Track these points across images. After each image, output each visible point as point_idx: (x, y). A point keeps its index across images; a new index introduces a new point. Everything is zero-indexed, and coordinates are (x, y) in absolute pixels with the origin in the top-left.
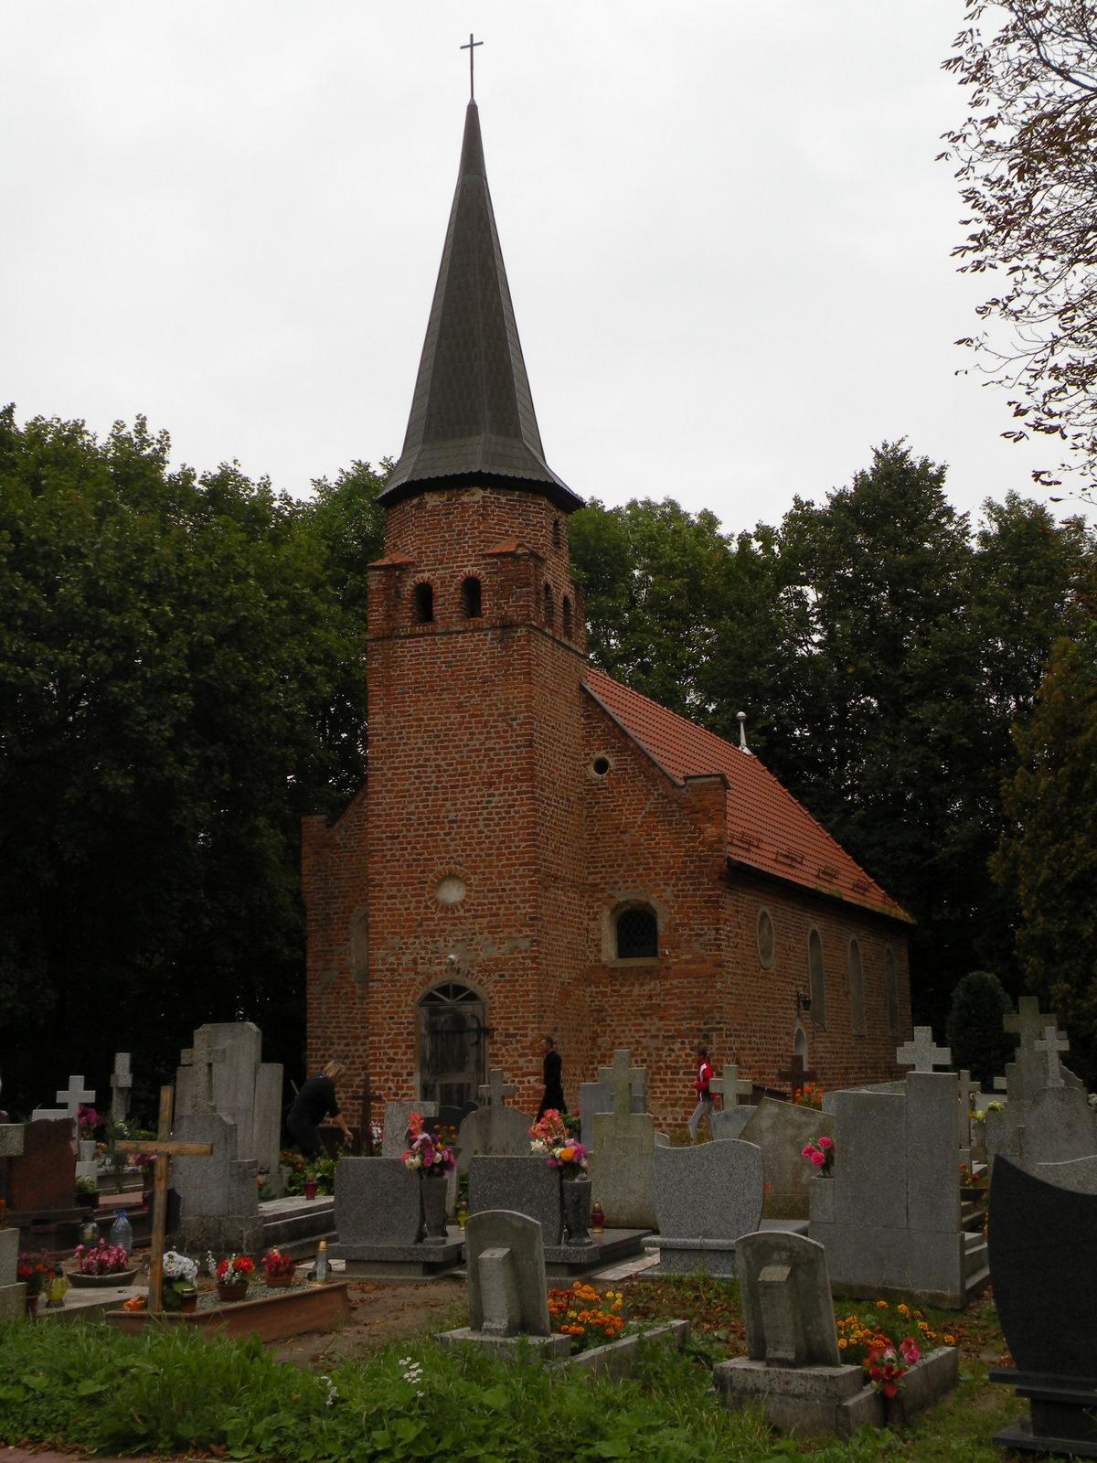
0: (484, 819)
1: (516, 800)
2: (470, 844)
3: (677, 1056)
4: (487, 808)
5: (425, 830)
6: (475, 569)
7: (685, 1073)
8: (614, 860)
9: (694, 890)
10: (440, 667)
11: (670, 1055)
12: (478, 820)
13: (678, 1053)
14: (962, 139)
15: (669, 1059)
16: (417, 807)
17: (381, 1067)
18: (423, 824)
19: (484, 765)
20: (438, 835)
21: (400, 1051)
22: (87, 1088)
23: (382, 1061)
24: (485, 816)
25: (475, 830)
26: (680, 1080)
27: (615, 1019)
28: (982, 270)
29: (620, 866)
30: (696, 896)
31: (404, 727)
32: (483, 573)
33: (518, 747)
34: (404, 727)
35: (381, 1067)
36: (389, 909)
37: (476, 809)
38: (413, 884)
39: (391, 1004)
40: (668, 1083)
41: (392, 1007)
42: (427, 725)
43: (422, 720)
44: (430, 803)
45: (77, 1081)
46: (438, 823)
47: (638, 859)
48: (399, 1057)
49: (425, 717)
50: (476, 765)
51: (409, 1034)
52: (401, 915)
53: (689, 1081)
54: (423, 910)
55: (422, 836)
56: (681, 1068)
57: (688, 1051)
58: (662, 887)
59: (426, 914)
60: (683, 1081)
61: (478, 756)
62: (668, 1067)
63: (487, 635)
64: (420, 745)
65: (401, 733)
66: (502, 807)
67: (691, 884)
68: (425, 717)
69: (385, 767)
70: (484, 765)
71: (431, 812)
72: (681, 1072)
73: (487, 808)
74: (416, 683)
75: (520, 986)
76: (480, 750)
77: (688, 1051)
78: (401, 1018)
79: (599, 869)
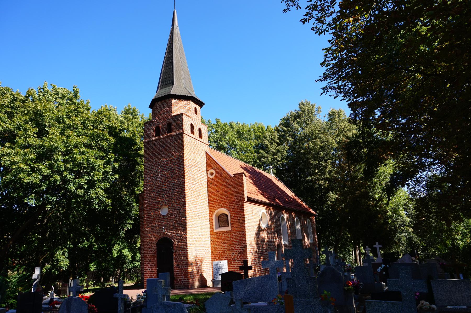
0: (173, 189)
1: (181, 183)
2: (169, 197)
3: (235, 256)
4: (173, 186)
5: (158, 194)
6: (170, 120)
7: (237, 261)
8: (216, 200)
9: (237, 206)
10: (161, 148)
11: (233, 255)
12: (171, 190)
13: (235, 255)
14: (317, 16)
15: (233, 256)
16: (156, 187)
17: (147, 263)
18: (157, 192)
19: (173, 174)
20: (161, 195)
21: (152, 258)
22: (379, 244)
23: (147, 261)
24: (173, 188)
25: (170, 193)
26: (236, 263)
27: (218, 245)
28: (286, 12)
29: (217, 201)
30: (238, 208)
31: (152, 165)
32: (172, 121)
33: (181, 168)
34: (152, 165)
35: (147, 263)
36: (149, 217)
37: (171, 186)
38: (155, 209)
39: (150, 245)
40: (233, 264)
41: (150, 245)
42: (159, 164)
43: (157, 163)
44: (159, 186)
45: (377, 243)
46: (161, 191)
47: (222, 199)
48: (152, 260)
49: (158, 162)
50: (171, 174)
51: (154, 253)
52: (152, 218)
53: (239, 263)
54: (157, 217)
55: (157, 195)
56: (236, 259)
57: (238, 254)
58: (229, 206)
59: (158, 218)
60: (237, 263)
61: (171, 171)
62: (233, 259)
63: (173, 138)
64: (156, 170)
65: (152, 167)
66: (177, 185)
67: (237, 205)
68: (158, 162)
69: (148, 177)
70: (173, 174)
71: (159, 189)
72: (236, 260)
73: (173, 186)
74: (156, 153)
75: (148, 239)
76: (171, 170)
77: (238, 254)
78: (152, 249)
79: (212, 202)
